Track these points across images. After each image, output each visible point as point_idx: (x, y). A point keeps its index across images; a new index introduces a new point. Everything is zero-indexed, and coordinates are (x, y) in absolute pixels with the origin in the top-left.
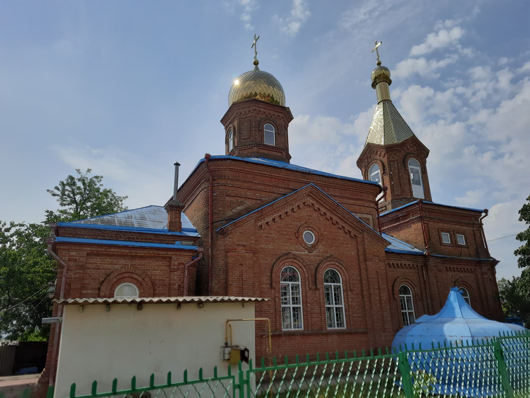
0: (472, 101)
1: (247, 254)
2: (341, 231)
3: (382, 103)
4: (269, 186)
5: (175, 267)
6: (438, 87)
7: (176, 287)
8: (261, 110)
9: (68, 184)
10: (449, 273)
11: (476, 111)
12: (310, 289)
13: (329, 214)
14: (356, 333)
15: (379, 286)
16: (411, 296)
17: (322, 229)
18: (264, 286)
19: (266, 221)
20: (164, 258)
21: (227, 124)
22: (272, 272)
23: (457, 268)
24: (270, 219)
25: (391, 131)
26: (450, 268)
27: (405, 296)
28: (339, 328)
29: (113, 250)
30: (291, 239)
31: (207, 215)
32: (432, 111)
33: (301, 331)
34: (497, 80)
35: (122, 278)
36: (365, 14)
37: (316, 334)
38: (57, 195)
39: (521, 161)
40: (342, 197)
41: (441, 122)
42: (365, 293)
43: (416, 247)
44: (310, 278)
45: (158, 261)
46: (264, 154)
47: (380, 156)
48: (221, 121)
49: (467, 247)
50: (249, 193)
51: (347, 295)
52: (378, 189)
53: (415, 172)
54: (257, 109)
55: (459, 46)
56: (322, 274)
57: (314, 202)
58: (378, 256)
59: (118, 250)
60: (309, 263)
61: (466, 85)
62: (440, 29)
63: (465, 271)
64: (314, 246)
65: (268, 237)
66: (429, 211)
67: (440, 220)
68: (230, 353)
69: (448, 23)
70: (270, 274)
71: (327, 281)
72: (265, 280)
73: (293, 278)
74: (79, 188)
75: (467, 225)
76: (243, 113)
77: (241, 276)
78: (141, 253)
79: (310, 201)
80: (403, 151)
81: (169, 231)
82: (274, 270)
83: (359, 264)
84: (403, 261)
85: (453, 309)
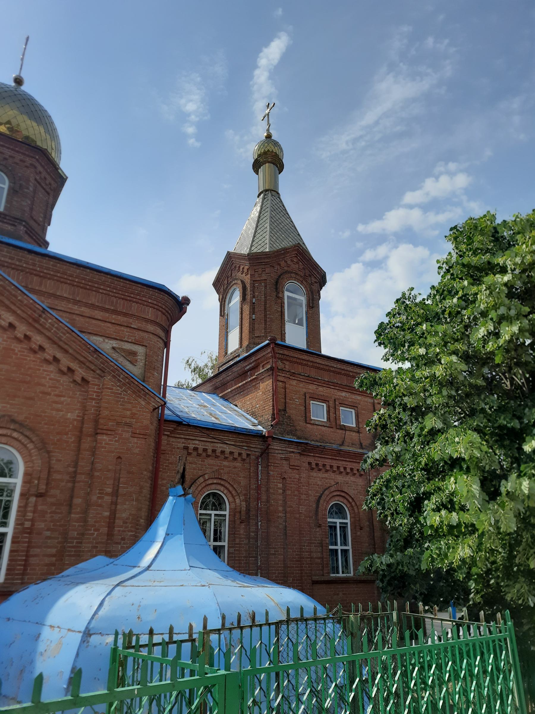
2: (52, 368)
10: (314, 474)
16: (348, 521)
23: (331, 467)
25: (265, 234)
26: (317, 465)
36: (347, 143)
42: (77, 501)
43: (260, 424)
49: (358, 431)
51: (26, 506)
55: (464, 198)
58: (129, 425)
62: (441, 174)
66: (291, 362)
67: (311, 380)
69: (452, 166)
83: (79, 440)
84: (219, 445)
85: (152, 542)
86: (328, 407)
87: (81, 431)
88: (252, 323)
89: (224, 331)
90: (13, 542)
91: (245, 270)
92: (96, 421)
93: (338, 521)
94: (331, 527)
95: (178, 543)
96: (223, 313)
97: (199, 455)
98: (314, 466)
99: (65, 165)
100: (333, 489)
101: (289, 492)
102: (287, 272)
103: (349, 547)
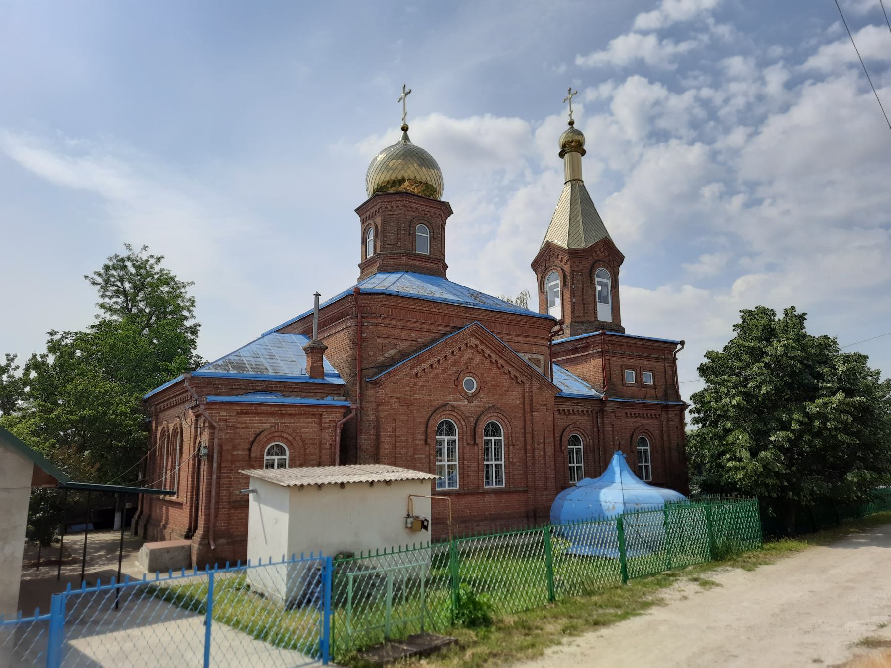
0: (722, 113)
3: (569, 183)
4: (426, 323)
5: (326, 425)
6: (673, 84)
7: (327, 446)
8: (414, 205)
11: (727, 130)
12: (468, 444)
13: (494, 356)
14: (515, 492)
16: (581, 447)
17: (485, 375)
18: (417, 442)
21: (364, 217)
22: (427, 427)
24: (426, 365)
27: (574, 447)
29: (263, 408)
31: (354, 359)
32: (663, 123)
33: (457, 491)
34: (762, 81)
37: (472, 494)
38: (99, 284)
39: (788, 212)
40: (511, 334)
41: (673, 142)
42: (528, 447)
43: (593, 388)
46: (415, 266)
47: (562, 261)
48: (357, 211)
49: (655, 387)
50: (403, 334)
52: (553, 323)
53: (604, 285)
55: (711, 21)
57: (478, 343)
59: (268, 408)
60: (468, 415)
61: (716, 85)
64: (474, 395)
67: (625, 355)
68: (412, 523)
70: (424, 429)
71: (487, 436)
72: (420, 435)
73: (450, 431)
75: (658, 360)
76: (389, 208)
78: (291, 410)
79: (473, 341)
80: (590, 258)
81: (310, 378)
82: (430, 425)
83: (524, 415)
85: (614, 473)
86: (636, 373)
89: (545, 306)
97: (565, 413)
103: (650, 464)
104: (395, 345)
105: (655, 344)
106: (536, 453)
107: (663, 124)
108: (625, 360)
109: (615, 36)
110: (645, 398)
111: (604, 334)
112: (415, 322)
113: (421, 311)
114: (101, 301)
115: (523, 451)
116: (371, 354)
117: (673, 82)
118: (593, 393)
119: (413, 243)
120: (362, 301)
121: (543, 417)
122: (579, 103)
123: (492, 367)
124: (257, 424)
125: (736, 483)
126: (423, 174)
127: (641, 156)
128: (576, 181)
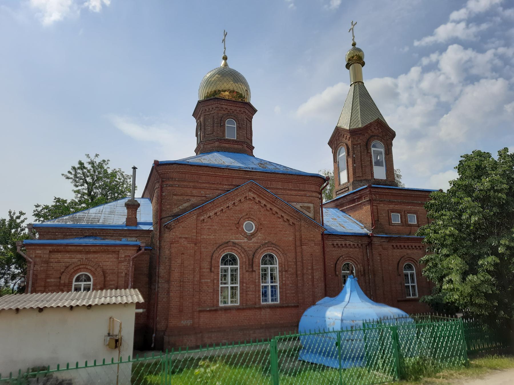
1: (189, 245)
2: (281, 220)
4: (213, 184)
5: (122, 259)
7: (123, 274)
8: (224, 106)
9: (79, 168)
10: (395, 251)
13: (269, 206)
15: (312, 267)
16: (414, 272)
17: (262, 219)
18: (204, 270)
19: (208, 216)
20: (114, 252)
22: (211, 259)
23: (404, 246)
26: (397, 246)
28: (273, 303)
29: (70, 248)
30: (231, 230)
35: (78, 269)
37: (250, 309)
38: (71, 178)
42: (299, 272)
43: (365, 227)
44: (247, 262)
45: (109, 254)
50: (195, 192)
51: (282, 275)
54: (219, 106)
55: (501, 9)
56: (259, 257)
57: (255, 196)
58: (314, 241)
59: (74, 248)
60: (247, 249)
63: (413, 249)
64: (253, 235)
65: (210, 229)
66: (379, 194)
67: (391, 202)
70: (209, 260)
72: (206, 265)
73: (233, 261)
74: (89, 171)
76: (207, 110)
77: (182, 263)
79: (251, 195)
81: (127, 225)
82: (214, 258)
84: (347, 242)
85: (346, 293)
87: (296, 245)
88: (354, 169)
89: (337, 172)
90: (280, 289)
91: (348, 138)
92: (301, 241)
93: (409, 272)
94: (405, 275)
95: (355, 295)
96: (335, 161)
97: (339, 247)
98: (395, 247)
99: (254, 102)
100: (406, 257)
101: (383, 261)
102: (372, 136)
103: (416, 284)
104: (187, 200)
105: (417, 193)
106: (305, 277)
107: (474, 71)
108: (391, 206)
109: (438, 25)
110: (410, 234)
111: (370, 187)
112: (203, 183)
113: (208, 175)
114: (76, 189)
115: (295, 276)
116: (168, 207)
117: (477, 45)
118: (365, 231)
119: (224, 132)
120: (161, 170)
121: (312, 249)
122: (419, 66)
123: (268, 213)
124: (66, 258)
125: (455, 303)
126: (238, 88)
127: (461, 91)
128: (359, 85)
